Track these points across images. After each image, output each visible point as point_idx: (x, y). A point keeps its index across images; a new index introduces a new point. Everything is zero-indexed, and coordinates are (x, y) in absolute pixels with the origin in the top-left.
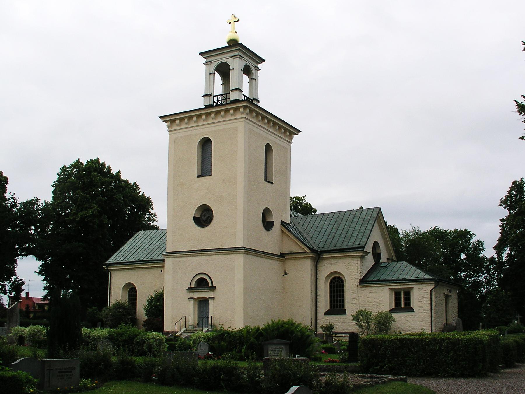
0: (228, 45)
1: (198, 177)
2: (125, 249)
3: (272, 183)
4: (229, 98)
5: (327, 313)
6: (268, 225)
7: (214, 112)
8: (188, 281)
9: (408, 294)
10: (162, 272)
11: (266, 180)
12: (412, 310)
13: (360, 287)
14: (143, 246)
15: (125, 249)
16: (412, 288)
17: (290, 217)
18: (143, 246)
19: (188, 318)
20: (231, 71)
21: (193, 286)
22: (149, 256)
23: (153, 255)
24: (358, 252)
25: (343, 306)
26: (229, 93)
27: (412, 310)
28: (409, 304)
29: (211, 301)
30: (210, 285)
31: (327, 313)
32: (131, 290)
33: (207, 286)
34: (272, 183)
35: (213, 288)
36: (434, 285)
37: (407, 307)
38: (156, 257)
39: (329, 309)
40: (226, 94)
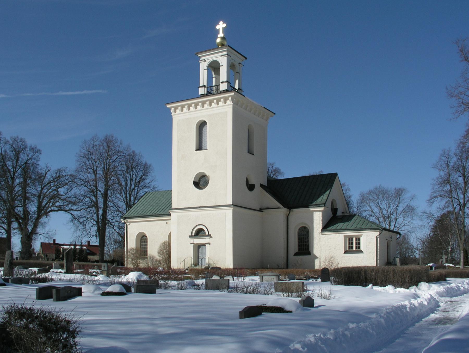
0: (266, 185)
1: (196, 150)
2: (137, 206)
3: (254, 155)
4: (220, 89)
5: (296, 254)
6: (251, 187)
7: (319, 265)
8: (189, 229)
9: (358, 239)
10: (167, 223)
11: (249, 152)
12: (361, 252)
13: (322, 235)
14: (152, 203)
15: (137, 206)
16: (362, 235)
17: (257, 295)
18: (152, 203)
19: (186, 260)
20: (221, 67)
21: (193, 234)
22: (164, 210)
23: (160, 211)
24: (320, 208)
25: (308, 249)
26: (220, 85)
27: (361, 252)
28: (359, 248)
29: (207, 245)
30: (207, 234)
31: (296, 254)
32: (143, 239)
33: (204, 235)
34: (254, 155)
35: (209, 236)
36: (379, 232)
37: (358, 249)
38: (162, 212)
39: (297, 251)
40: (217, 86)
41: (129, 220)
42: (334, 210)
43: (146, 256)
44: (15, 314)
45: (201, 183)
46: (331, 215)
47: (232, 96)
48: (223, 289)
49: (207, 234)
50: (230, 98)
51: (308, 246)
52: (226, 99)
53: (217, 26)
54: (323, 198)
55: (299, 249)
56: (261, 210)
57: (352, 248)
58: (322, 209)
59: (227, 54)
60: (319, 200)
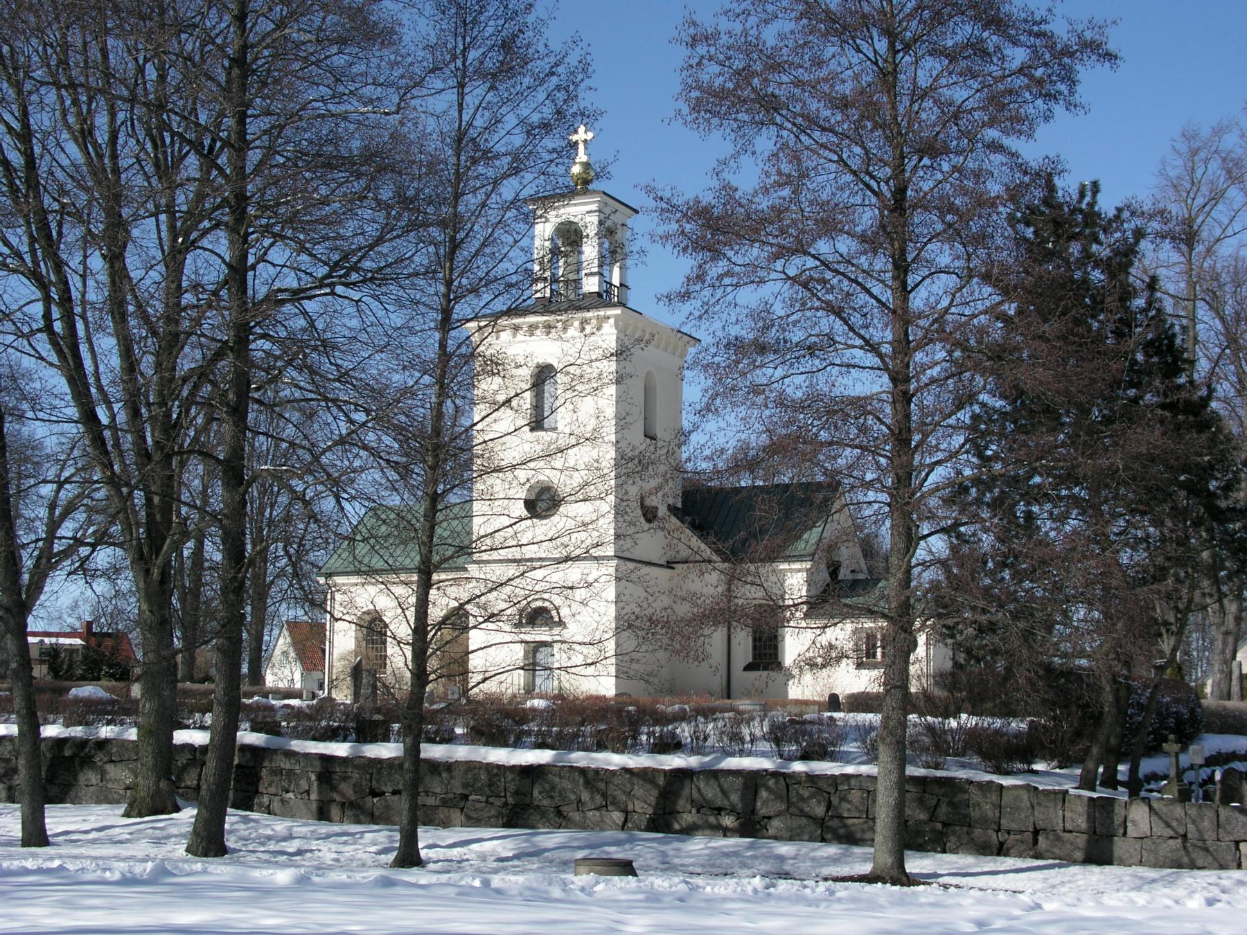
5: (748, 668)
6: (650, 515)
25: (776, 655)
30: (556, 619)
31: (748, 668)
41: (339, 580)
42: (834, 569)
43: (870, 637)
44: (396, 726)
45: (543, 505)
46: (824, 576)
47: (616, 317)
48: (776, 637)
49: (556, 619)
50: (612, 321)
51: (776, 648)
52: (602, 320)
53: (787, 692)
54: (812, 536)
55: (754, 658)
56: (669, 565)
57: (874, 655)
58: (808, 565)
59: (599, 211)
60: (801, 545)
